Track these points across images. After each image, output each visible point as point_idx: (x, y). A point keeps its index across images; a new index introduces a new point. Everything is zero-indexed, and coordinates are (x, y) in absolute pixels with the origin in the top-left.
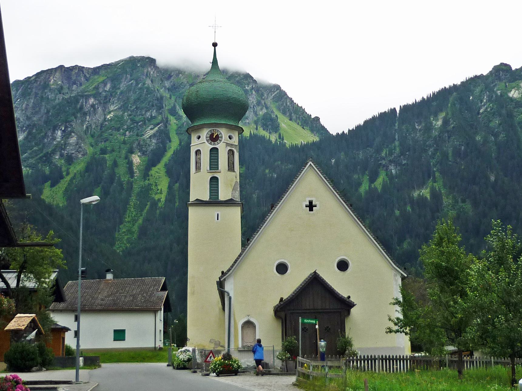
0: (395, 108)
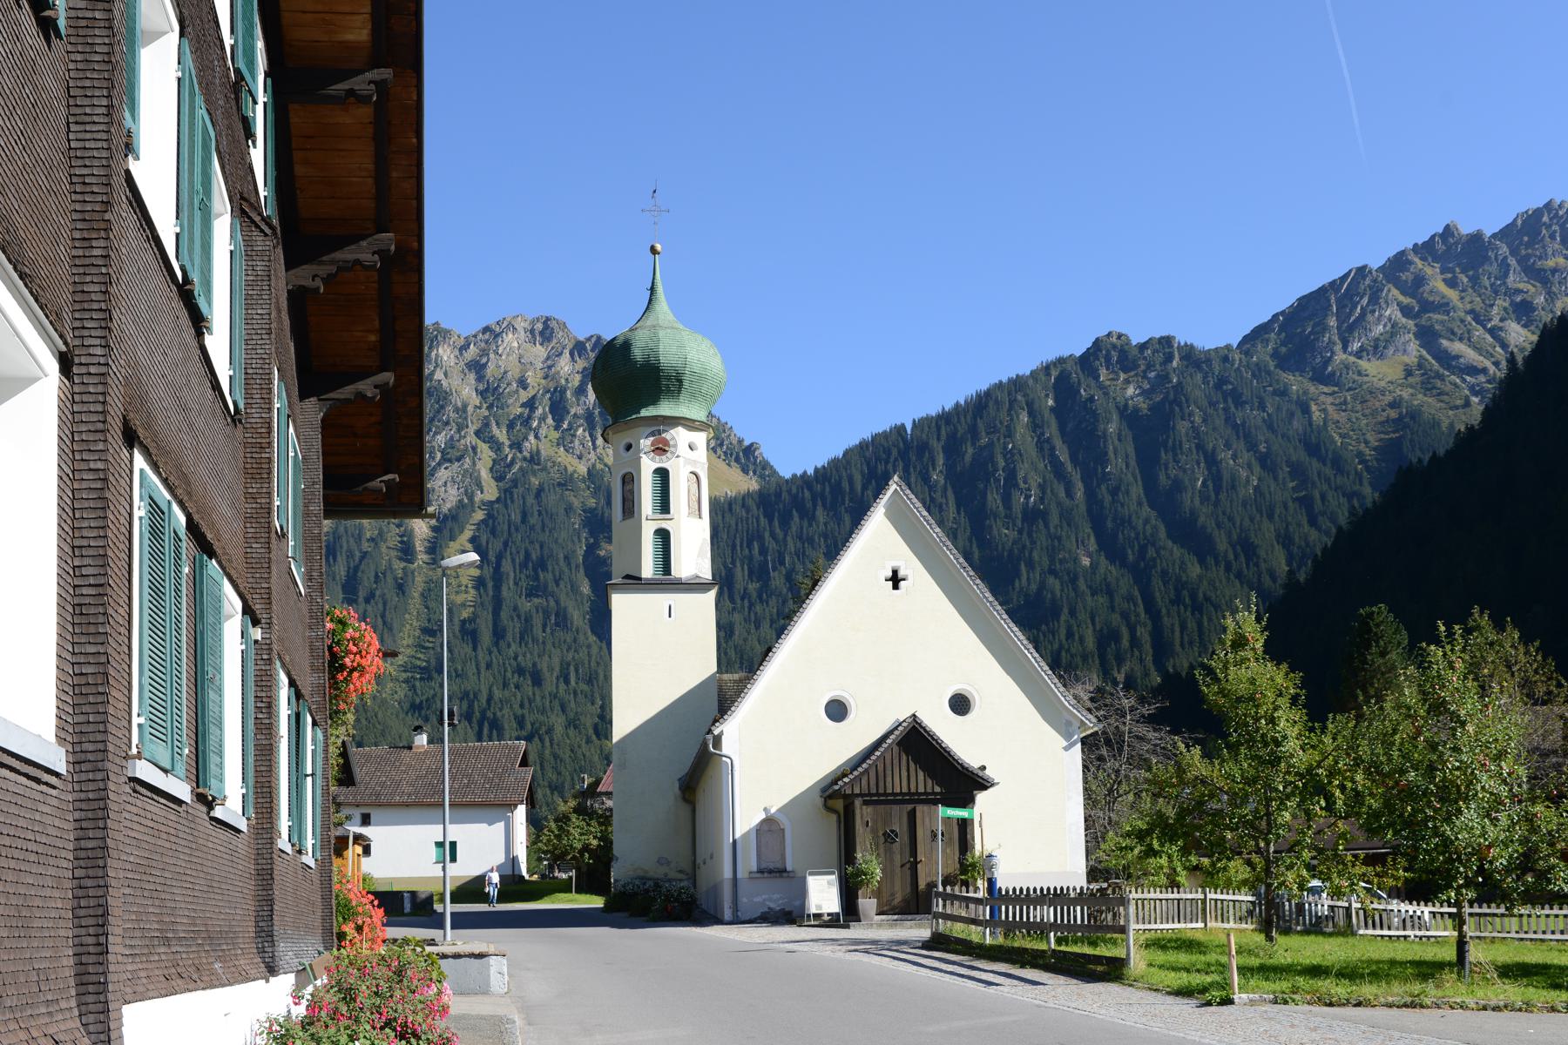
0: (903, 426)
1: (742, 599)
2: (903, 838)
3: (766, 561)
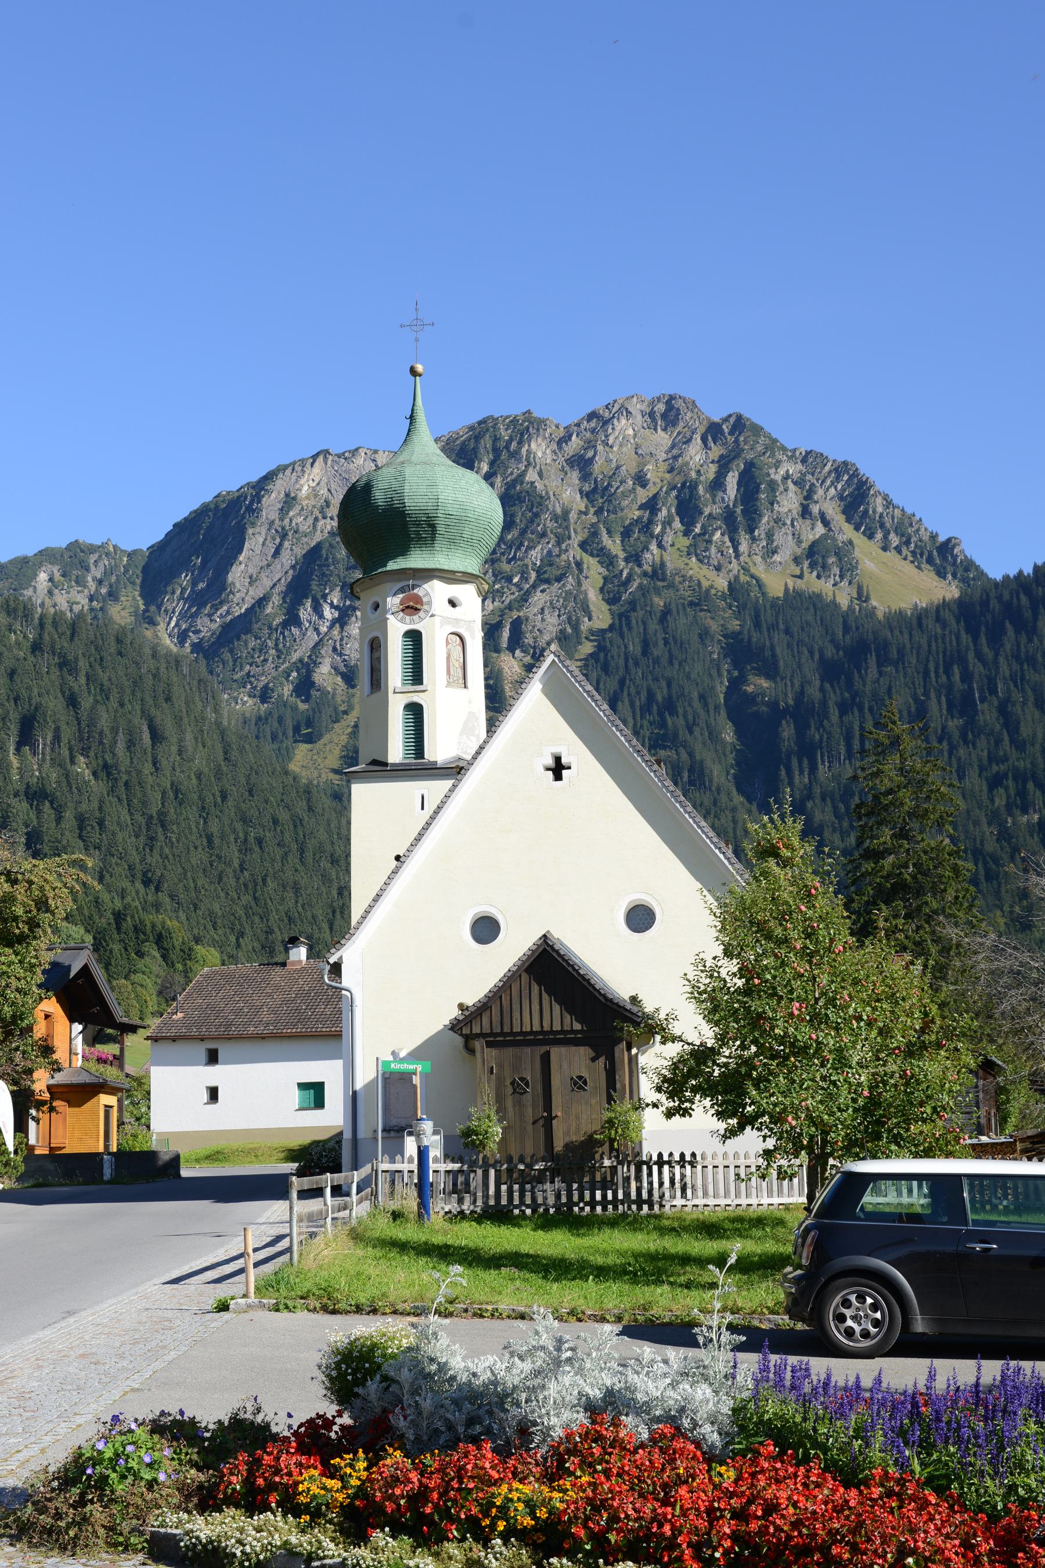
1: (940, 741)
2: (534, 1089)
3: (971, 689)
